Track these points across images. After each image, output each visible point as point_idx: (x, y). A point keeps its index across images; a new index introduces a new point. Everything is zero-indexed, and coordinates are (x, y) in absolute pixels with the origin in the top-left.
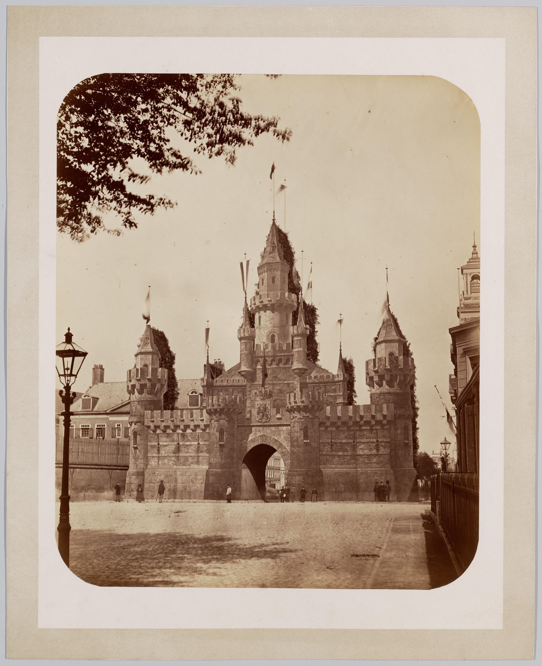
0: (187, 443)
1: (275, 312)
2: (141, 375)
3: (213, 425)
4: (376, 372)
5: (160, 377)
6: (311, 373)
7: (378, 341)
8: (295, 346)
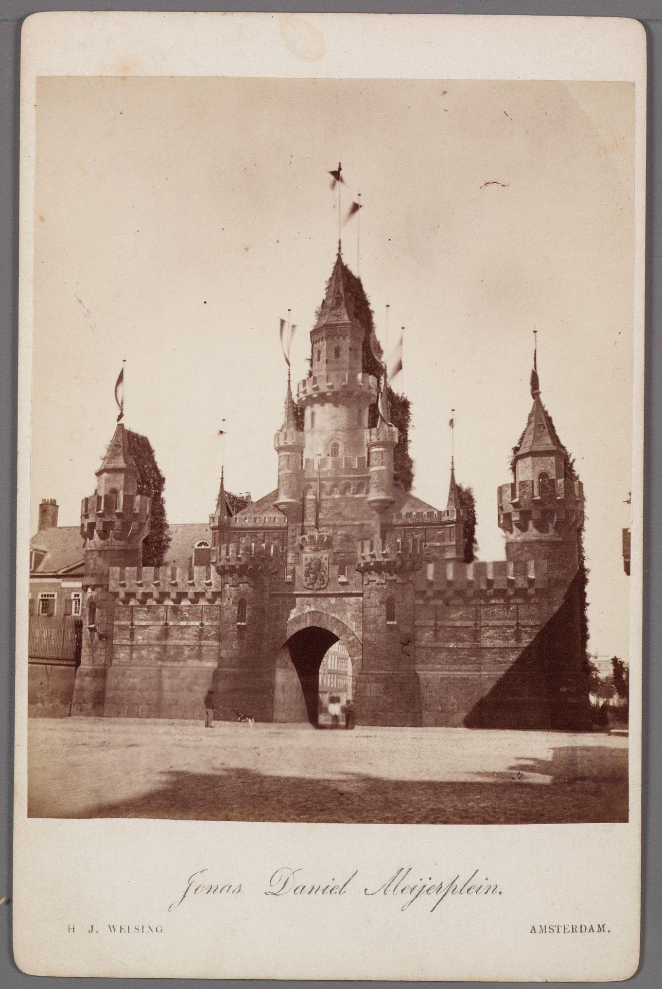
0: (183, 623)
1: (340, 406)
2: (105, 506)
3: (228, 594)
4: (516, 505)
5: (137, 511)
6: (400, 508)
7: (519, 453)
8: (372, 461)
